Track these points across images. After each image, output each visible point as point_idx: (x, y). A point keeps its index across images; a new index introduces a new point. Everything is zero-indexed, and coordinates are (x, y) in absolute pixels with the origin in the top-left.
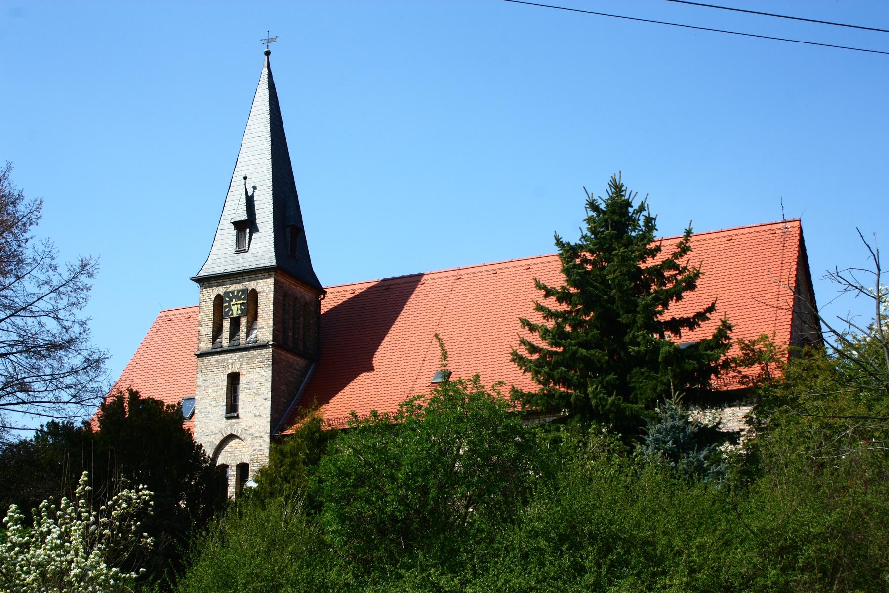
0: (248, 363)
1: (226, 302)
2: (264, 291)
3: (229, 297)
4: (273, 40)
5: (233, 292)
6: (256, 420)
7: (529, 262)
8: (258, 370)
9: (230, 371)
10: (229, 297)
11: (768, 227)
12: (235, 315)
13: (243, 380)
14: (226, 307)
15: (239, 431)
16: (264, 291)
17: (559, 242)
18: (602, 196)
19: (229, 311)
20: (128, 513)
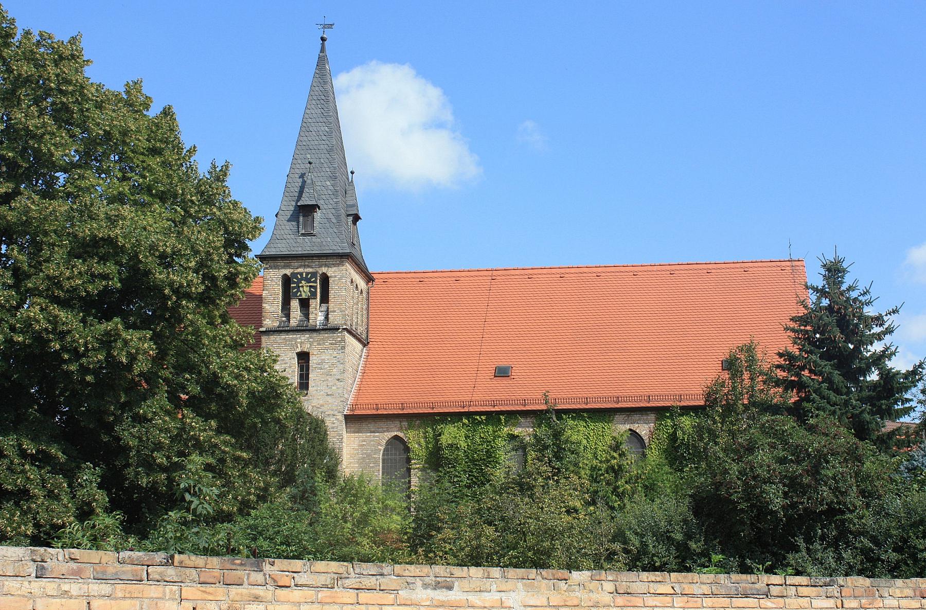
0: (319, 344)
1: (294, 283)
2: (335, 276)
3: (297, 278)
4: (330, 26)
5: (301, 274)
6: (329, 399)
7: (562, 271)
8: (330, 352)
9: (299, 350)
10: (297, 278)
11: (779, 264)
12: (304, 296)
13: (313, 360)
14: (294, 288)
15: (310, 408)
16: (335, 276)
17: (834, 271)
18: (220, 164)
19: (297, 292)
20: (887, 398)
